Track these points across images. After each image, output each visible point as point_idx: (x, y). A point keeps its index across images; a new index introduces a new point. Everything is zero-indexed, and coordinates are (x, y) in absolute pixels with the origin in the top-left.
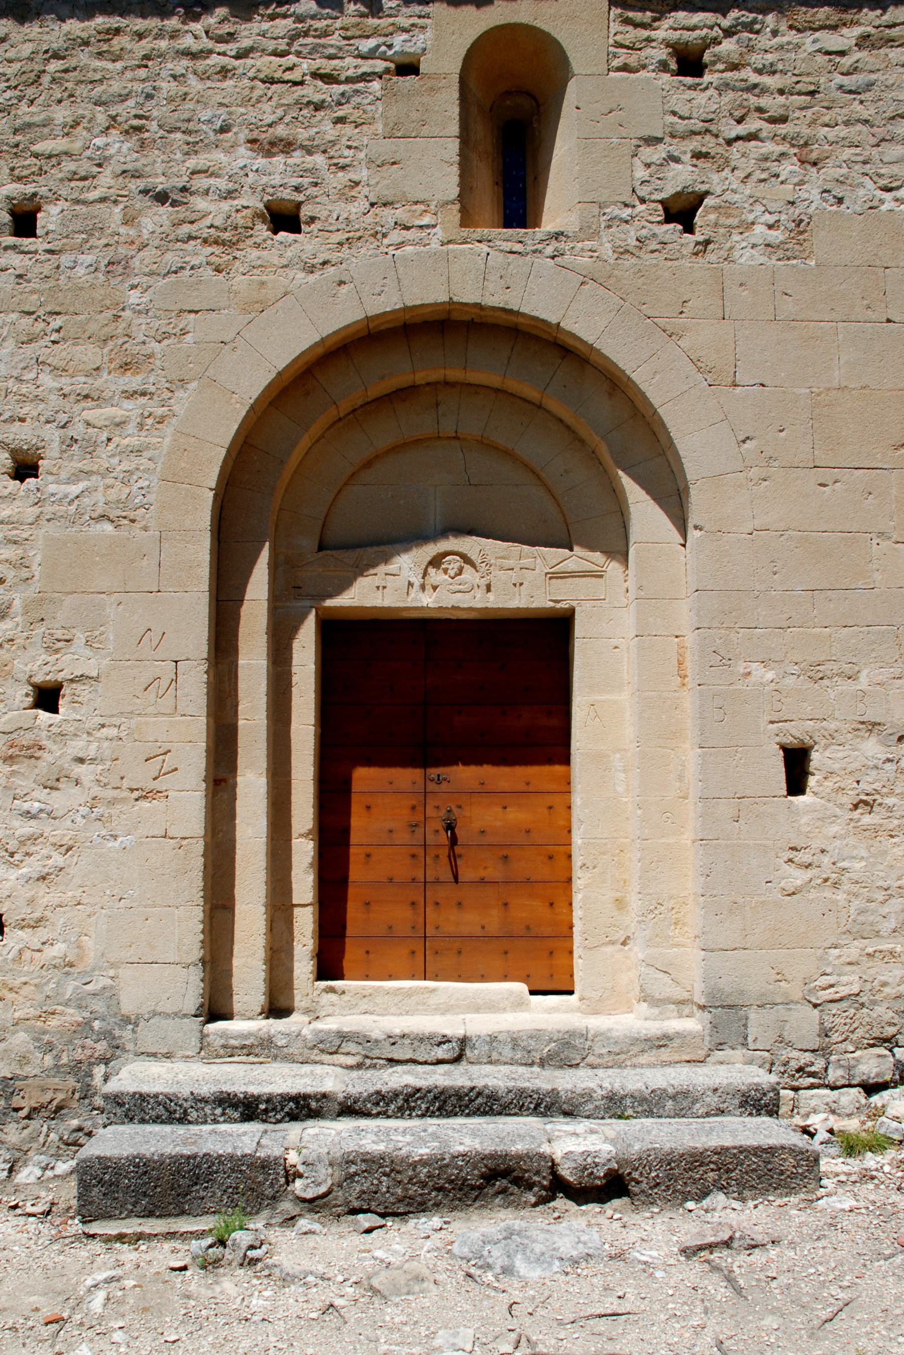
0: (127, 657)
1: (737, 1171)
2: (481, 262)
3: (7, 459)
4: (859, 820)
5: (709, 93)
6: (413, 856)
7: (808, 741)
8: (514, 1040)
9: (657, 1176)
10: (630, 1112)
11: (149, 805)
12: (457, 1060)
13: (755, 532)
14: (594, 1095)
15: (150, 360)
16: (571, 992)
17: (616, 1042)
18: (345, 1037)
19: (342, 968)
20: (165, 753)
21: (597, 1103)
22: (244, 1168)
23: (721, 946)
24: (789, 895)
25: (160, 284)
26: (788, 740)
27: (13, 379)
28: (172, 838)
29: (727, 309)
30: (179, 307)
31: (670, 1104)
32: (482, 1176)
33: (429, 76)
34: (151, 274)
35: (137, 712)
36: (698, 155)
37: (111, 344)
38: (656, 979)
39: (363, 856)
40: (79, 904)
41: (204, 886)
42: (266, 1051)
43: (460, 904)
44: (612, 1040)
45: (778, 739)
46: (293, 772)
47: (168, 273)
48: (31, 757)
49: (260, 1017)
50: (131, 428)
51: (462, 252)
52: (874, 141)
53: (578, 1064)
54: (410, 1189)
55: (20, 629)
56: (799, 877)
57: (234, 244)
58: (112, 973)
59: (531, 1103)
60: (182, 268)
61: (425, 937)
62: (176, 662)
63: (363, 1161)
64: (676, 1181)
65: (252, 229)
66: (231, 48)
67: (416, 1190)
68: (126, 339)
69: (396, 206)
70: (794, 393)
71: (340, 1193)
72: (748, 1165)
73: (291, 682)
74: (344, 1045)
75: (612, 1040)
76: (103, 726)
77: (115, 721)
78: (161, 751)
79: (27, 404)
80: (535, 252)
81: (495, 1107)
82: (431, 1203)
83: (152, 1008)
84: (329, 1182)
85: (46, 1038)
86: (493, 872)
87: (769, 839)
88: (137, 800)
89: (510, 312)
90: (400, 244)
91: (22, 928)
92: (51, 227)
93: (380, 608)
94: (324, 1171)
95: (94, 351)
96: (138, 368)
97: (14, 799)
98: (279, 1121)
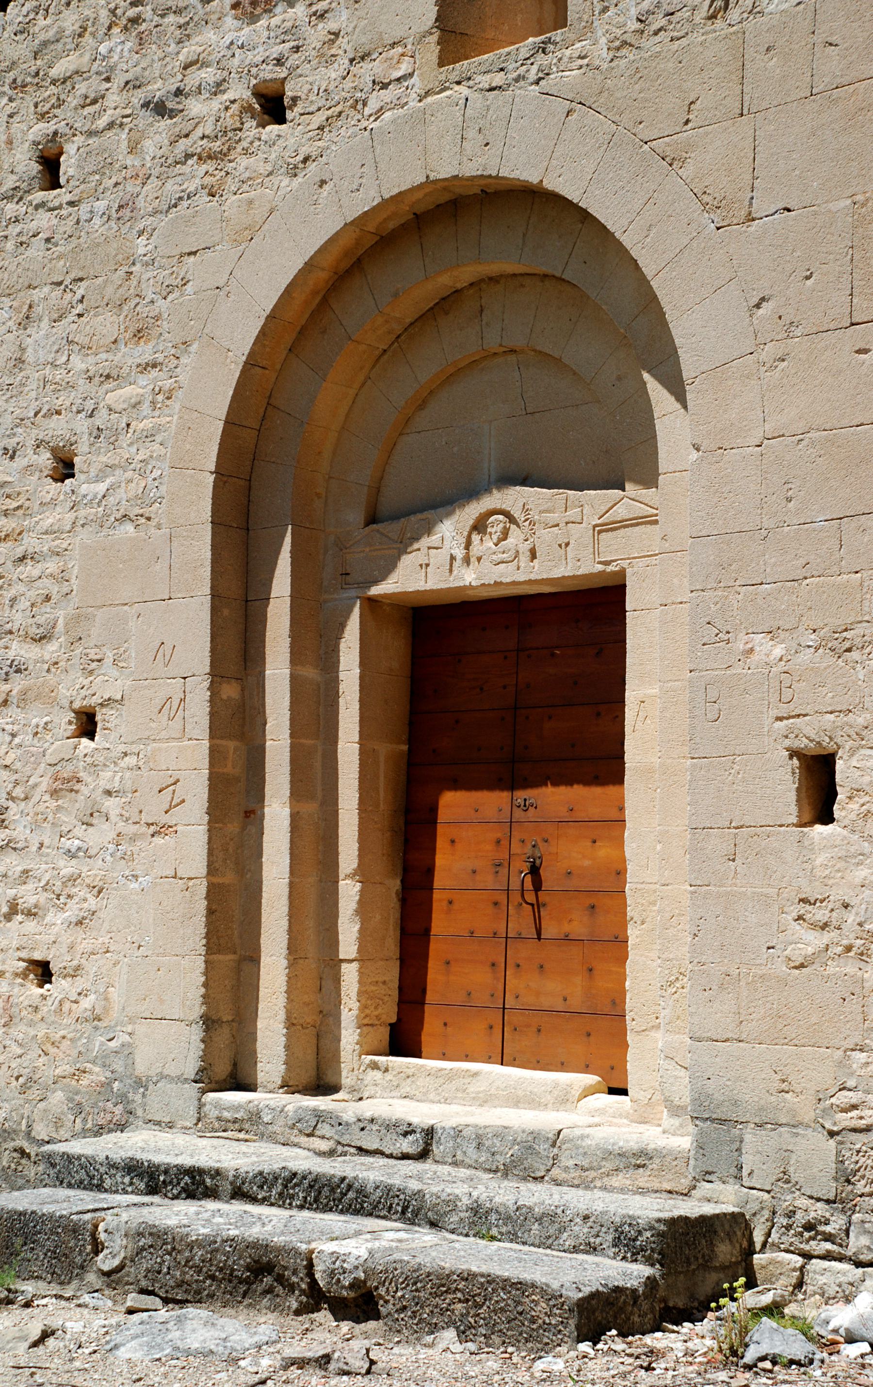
0: (145, 676)
1: (485, 1308)
2: (458, 112)
3: (48, 459)
6: (496, 904)
7: (831, 747)
8: (478, 1136)
9: (403, 1296)
10: (494, 1232)
11: (163, 841)
12: (423, 1155)
13: (766, 441)
14: (459, 1204)
15: (159, 323)
17: (585, 1153)
18: (320, 1117)
19: (419, 1043)
20: (175, 783)
21: (462, 1215)
22: (60, 1230)
23: (709, 1035)
24: (796, 968)
25: (163, 224)
27: (49, 366)
28: (181, 879)
29: (746, 98)
30: (176, 252)
32: (248, 1268)
34: (156, 212)
35: (152, 738)
37: (126, 307)
38: (676, 1077)
39: (445, 903)
40: (108, 952)
41: (207, 933)
42: (255, 1127)
43: (542, 967)
44: (581, 1150)
45: (787, 743)
46: (340, 799)
47: (169, 208)
48: (72, 790)
49: (281, 1091)
50: (146, 408)
51: (439, 103)
53: (543, 1177)
54: (187, 1273)
55: (63, 650)
56: (813, 941)
57: (225, 155)
58: (129, 1029)
59: (398, 1204)
60: (181, 198)
61: (504, 1008)
62: (185, 678)
63: (151, 1234)
64: (422, 1307)
65: (241, 130)
67: (192, 1276)
68: (137, 300)
69: (373, 57)
70: (830, 211)
71: (132, 1270)
72: (497, 1302)
73: (338, 692)
74: (319, 1126)
75: (581, 1150)
76: (126, 754)
77: (135, 748)
78: (172, 780)
79: (62, 393)
80: (517, 80)
81: (365, 1205)
82: (206, 1292)
83: (160, 1070)
84: (122, 1255)
86: (578, 926)
87: (773, 887)
88: (153, 836)
90: (378, 111)
91: (65, 977)
93: (422, 591)
94: (119, 1241)
95: (111, 319)
96: (149, 334)
97: (61, 836)
98: (175, 1197)
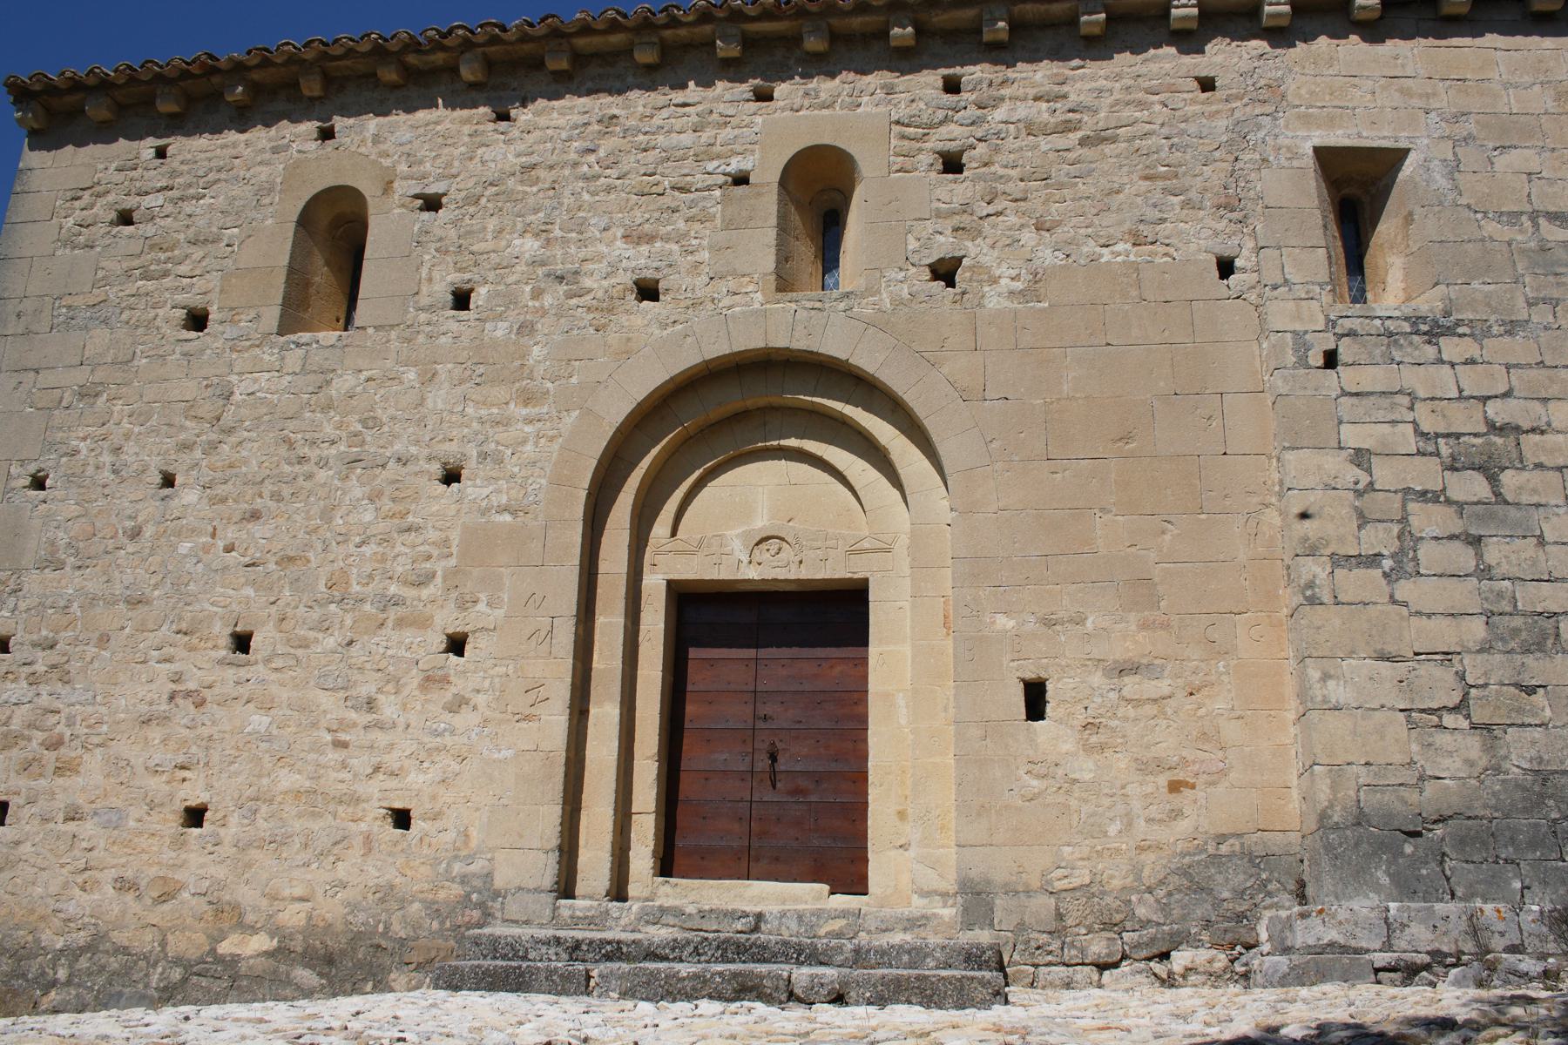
4: (1087, 739)
5: (965, 184)
7: (1043, 675)
16: (866, 894)
26: (1030, 675)
31: (906, 958)
33: (756, 185)
36: (956, 230)
45: (1019, 674)
52: (1094, 211)
58: (489, 856)
66: (614, 173)
85: (436, 906)
89: (812, 352)
92: (480, 303)
